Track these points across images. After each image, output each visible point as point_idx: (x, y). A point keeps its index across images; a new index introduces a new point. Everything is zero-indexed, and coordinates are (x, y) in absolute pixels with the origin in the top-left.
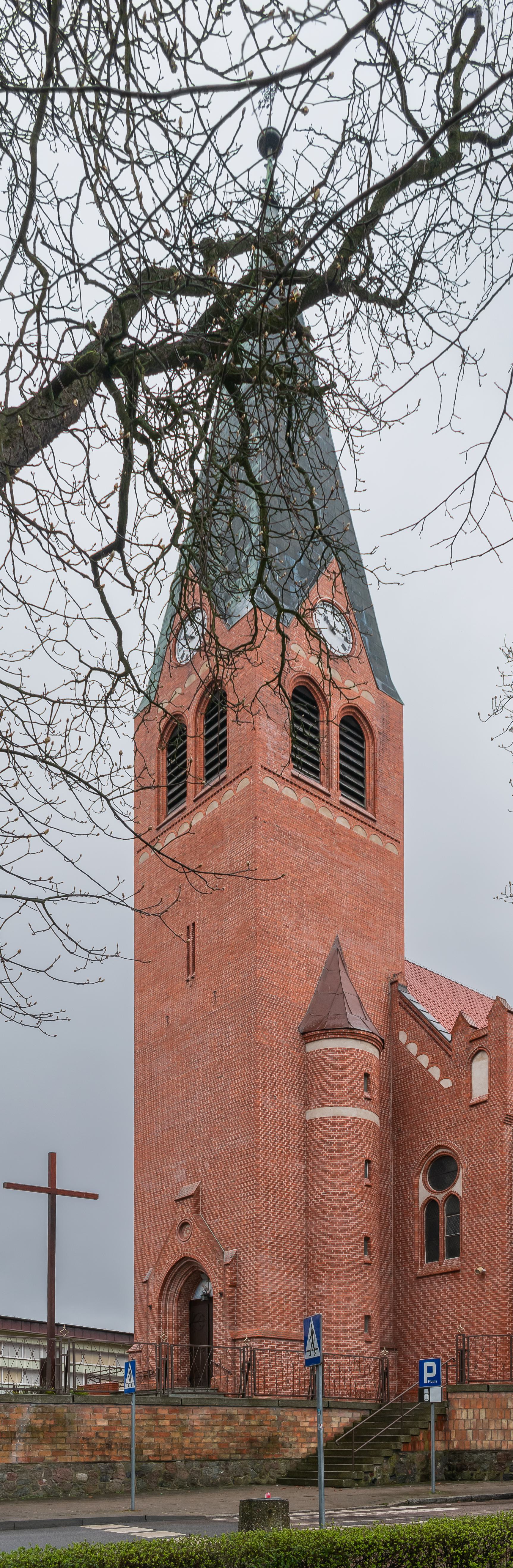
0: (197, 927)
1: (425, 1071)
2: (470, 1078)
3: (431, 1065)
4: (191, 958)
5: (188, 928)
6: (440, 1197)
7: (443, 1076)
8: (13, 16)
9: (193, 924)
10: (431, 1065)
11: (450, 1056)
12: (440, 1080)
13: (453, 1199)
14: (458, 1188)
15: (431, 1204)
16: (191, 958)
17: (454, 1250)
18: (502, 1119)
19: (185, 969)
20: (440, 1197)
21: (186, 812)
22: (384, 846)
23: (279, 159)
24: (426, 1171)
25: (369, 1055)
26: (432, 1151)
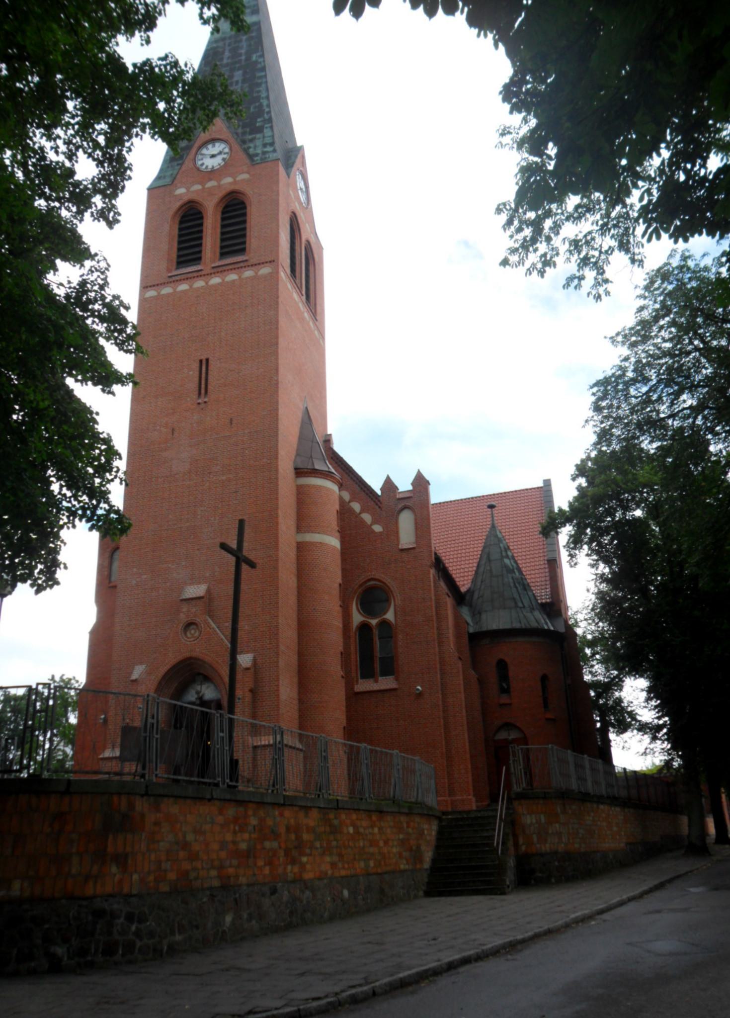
0: (211, 362)
1: (357, 516)
2: (397, 528)
3: (362, 511)
4: (203, 386)
5: (201, 361)
6: (374, 622)
7: (375, 522)
8: (716, 323)
9: (207, 360)
10: (362, 511)
11: (380, 507)
12: (371, 525)
13: (385, 624)
14: (390, 616)
15: (364, 628)
16: (203, 386)
17: (389, 667)
18: (429, 564)
19: (197, 392)
20: (374, 622)
21: (200, 273)
22: (159, 293)
23: (665, 260)
24: (357, 600)
25: (334, 492)
26: (369, 580)
